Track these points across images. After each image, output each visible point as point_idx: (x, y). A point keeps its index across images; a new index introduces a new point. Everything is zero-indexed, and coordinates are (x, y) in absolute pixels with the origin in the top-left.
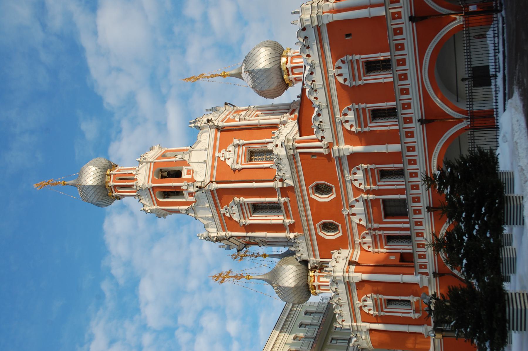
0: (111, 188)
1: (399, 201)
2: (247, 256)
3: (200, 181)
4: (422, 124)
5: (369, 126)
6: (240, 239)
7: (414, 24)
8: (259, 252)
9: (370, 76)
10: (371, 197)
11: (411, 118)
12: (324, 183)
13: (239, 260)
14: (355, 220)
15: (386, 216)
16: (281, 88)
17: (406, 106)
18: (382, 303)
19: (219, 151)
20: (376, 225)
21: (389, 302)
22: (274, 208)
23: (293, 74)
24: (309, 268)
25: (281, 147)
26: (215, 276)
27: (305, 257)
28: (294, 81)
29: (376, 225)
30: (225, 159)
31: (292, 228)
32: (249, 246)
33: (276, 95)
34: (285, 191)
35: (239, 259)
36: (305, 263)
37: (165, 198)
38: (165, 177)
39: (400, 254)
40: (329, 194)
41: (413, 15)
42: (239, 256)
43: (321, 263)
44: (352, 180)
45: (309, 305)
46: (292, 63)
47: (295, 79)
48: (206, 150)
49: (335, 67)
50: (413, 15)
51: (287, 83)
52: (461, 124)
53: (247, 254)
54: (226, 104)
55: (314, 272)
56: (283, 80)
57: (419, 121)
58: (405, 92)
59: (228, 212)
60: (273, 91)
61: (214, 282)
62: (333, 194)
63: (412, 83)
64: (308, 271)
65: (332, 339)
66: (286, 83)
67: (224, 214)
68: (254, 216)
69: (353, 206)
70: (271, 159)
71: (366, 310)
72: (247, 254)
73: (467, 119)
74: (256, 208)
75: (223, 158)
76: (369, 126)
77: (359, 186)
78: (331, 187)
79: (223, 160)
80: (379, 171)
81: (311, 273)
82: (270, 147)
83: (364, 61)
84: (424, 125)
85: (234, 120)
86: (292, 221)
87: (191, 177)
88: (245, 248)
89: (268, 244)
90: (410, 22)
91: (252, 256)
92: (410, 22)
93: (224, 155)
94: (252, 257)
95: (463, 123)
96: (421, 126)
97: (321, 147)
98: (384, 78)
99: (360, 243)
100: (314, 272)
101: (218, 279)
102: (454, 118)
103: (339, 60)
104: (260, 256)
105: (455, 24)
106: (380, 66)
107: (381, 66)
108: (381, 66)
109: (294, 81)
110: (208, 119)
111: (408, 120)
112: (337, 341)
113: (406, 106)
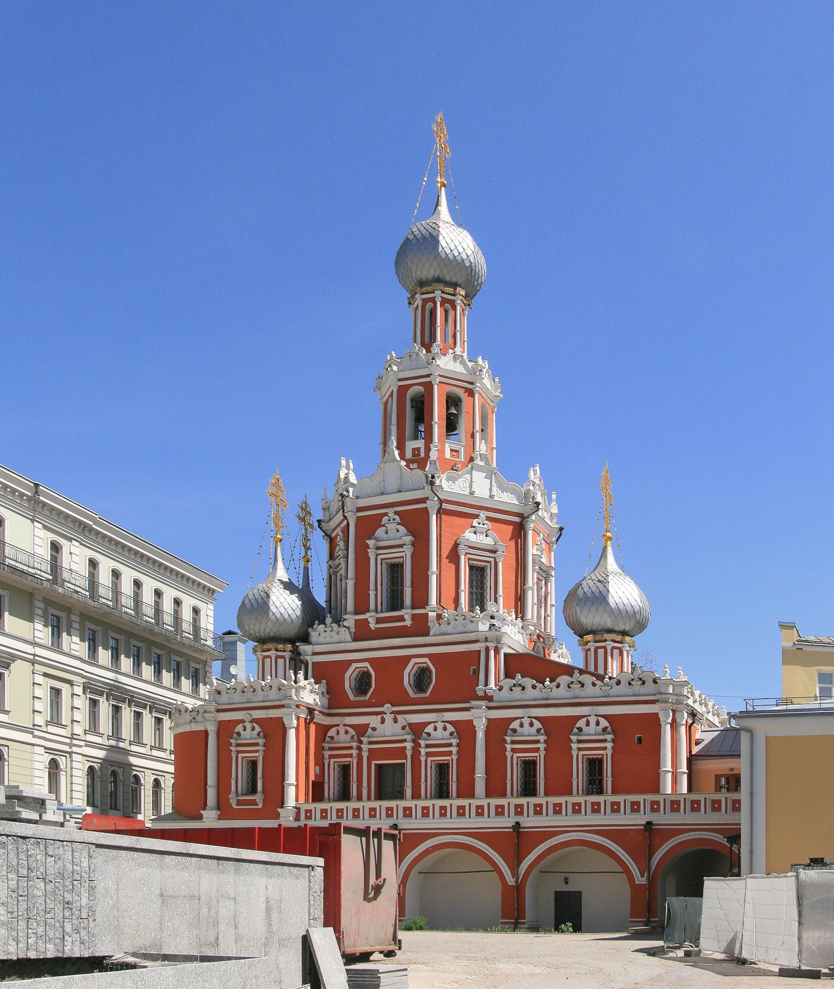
0: (431, 293)
1: (402, 785)
2: (306, 529)
3: (442, 483)
4: (513, 827)
5: (512, 755)
6: (343, 532)
7: (642, 827)
8: (311, 549)
9: (583, 762)
10: (409, 753)
11: (521, 813)
12: (431, 681)
13: (299, 515)
14: (374, 721)
15: (379, 767)
16: (577, 627)
17: (356, 813)
18: (709, 829)
19: (488, 519)
20: (365, 755)
21: (253, 764)
22: (395, 602)
23: (597, 648)
24: (297, 644)
25: (490, 624)
26: (306, 506)
27: (314, 635)
28: (587, 647)
29: (365, 755)
30: (474, 527)
31: (362, 625)
32: (327, 539)
33: (568, 618)
34: (421, 627)
35: (301, 515)
36: (305, 638)
37: (412, 400)
38: (448, 409)
39: (322, 781)
40: (415, 687)
41: (653, 827)
42: (306, 514)
43: (305, 662)
44: (436, 723)
45: (72, 552)
46: (613, 648)
47: (589, 649)
48: (492, 497)
49: (600, 718)
50: (653, 827)
51: (584, 637)
52: (510, 875)
53: (309, 529)
54: (561, 529)
55: (290, 651)
56: (588, 633)
57: (518, 823)
58: (480, 811)
59: (390, 522)
60: (574, 615)
61: (299, 505)
62: (415, 693)
63: (566, 820)
64: (292, 641)
65: (117, 640)
66: (585, 635)
67: (386, 514)
68: (381, 564)
69: (395, 721)
70: (472, 609)
71: (239, 728)
72: (309, 529)
73: (517, 881)
74: (395, 570)
75: (477, 525)
76: (512, 755)
77: (425, 733)
78: (425, 691)
79: (474, 525)
80: (448, 762)
81: (289, 647)
82: (491, 607)
83: (603, 757)
84: (512, 830)
85: (534, 543)
86: (373, 626)
87: (446, 457)
88: (324, 535)
89: (332, 577)
90: (645, 823)
91: (306, 539)
92: (645, 823)
93: (481, 525)
94: (304, 538)
95: (511, 878)
96: (511, 826)
97: (486, 684)
98: (578, 782)
99: (338, 725)
100: (290, 651)
101: (302, 509)
102: (518, 866)
103: (607, 724)
104: (306, 553)
105: (637, 875)
106: (595, 776)
107: (595, 778)
108: (595, 778)
109: (587, 647)
110: (540, 504)
111: (390, 812)
112: (92, 640)
113: (308, 814)
